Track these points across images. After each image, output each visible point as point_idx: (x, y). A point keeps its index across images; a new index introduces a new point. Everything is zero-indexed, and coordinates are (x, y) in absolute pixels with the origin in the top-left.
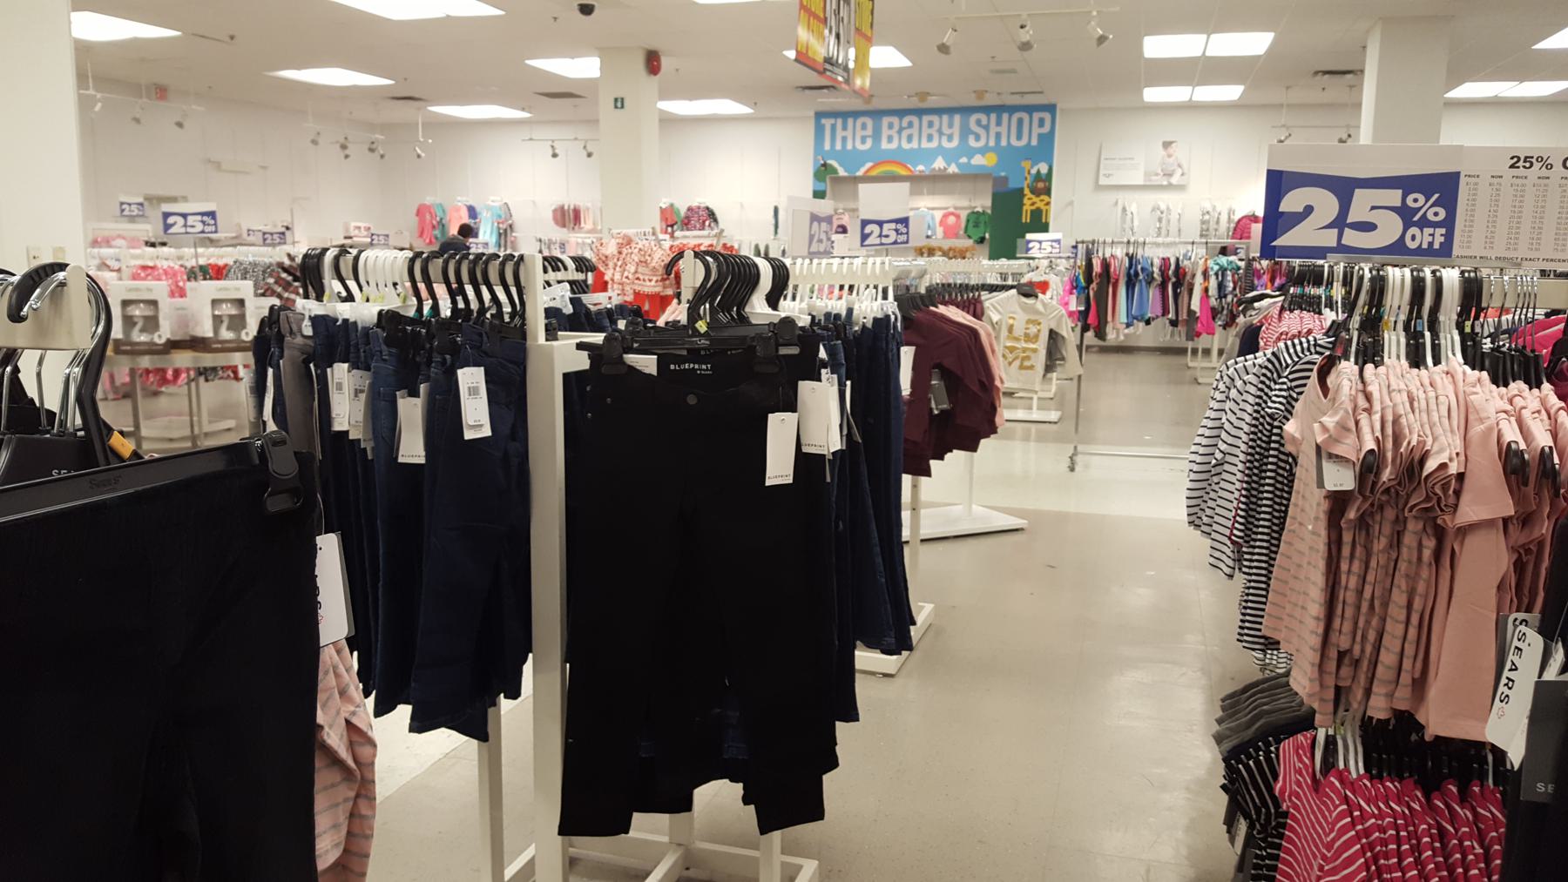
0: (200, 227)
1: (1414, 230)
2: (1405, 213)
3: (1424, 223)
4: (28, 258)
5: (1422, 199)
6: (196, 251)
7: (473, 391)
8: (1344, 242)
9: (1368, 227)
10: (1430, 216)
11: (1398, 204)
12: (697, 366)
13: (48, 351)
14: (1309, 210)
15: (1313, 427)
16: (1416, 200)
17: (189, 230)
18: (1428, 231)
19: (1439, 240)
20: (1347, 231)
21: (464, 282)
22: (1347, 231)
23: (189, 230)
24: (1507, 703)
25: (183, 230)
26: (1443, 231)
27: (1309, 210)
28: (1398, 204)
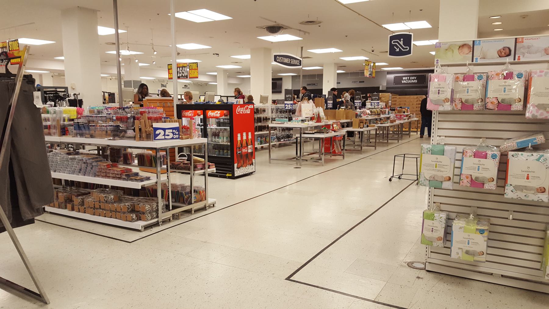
0: (376, 105)
1: (174, 135)
2: (173, 133)
3: (176, 134)
4: (453, 175)
5: (175, 131)
6: (119, 54)
7: (38, 97)
8: (165, 138)
9: (168, 135)
10: (176, 133)
11: (172, 132)
12: (9, 81)
13: (178, 123)
14: (160, 133)
15: (122, 103)
16: (174, 131)
17: (166, 137)
18: (176, 135)
19: (178, 137)
20: (166, 136)
21: (123, 85)
22: (166, 136)
23: (166, 137)
24: (465, 169)
25: (163, 137)
26: (178, 135)
27: (160, 133)
28: (172, 132)
